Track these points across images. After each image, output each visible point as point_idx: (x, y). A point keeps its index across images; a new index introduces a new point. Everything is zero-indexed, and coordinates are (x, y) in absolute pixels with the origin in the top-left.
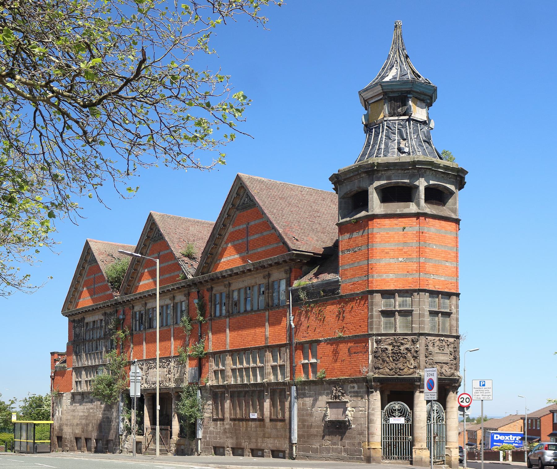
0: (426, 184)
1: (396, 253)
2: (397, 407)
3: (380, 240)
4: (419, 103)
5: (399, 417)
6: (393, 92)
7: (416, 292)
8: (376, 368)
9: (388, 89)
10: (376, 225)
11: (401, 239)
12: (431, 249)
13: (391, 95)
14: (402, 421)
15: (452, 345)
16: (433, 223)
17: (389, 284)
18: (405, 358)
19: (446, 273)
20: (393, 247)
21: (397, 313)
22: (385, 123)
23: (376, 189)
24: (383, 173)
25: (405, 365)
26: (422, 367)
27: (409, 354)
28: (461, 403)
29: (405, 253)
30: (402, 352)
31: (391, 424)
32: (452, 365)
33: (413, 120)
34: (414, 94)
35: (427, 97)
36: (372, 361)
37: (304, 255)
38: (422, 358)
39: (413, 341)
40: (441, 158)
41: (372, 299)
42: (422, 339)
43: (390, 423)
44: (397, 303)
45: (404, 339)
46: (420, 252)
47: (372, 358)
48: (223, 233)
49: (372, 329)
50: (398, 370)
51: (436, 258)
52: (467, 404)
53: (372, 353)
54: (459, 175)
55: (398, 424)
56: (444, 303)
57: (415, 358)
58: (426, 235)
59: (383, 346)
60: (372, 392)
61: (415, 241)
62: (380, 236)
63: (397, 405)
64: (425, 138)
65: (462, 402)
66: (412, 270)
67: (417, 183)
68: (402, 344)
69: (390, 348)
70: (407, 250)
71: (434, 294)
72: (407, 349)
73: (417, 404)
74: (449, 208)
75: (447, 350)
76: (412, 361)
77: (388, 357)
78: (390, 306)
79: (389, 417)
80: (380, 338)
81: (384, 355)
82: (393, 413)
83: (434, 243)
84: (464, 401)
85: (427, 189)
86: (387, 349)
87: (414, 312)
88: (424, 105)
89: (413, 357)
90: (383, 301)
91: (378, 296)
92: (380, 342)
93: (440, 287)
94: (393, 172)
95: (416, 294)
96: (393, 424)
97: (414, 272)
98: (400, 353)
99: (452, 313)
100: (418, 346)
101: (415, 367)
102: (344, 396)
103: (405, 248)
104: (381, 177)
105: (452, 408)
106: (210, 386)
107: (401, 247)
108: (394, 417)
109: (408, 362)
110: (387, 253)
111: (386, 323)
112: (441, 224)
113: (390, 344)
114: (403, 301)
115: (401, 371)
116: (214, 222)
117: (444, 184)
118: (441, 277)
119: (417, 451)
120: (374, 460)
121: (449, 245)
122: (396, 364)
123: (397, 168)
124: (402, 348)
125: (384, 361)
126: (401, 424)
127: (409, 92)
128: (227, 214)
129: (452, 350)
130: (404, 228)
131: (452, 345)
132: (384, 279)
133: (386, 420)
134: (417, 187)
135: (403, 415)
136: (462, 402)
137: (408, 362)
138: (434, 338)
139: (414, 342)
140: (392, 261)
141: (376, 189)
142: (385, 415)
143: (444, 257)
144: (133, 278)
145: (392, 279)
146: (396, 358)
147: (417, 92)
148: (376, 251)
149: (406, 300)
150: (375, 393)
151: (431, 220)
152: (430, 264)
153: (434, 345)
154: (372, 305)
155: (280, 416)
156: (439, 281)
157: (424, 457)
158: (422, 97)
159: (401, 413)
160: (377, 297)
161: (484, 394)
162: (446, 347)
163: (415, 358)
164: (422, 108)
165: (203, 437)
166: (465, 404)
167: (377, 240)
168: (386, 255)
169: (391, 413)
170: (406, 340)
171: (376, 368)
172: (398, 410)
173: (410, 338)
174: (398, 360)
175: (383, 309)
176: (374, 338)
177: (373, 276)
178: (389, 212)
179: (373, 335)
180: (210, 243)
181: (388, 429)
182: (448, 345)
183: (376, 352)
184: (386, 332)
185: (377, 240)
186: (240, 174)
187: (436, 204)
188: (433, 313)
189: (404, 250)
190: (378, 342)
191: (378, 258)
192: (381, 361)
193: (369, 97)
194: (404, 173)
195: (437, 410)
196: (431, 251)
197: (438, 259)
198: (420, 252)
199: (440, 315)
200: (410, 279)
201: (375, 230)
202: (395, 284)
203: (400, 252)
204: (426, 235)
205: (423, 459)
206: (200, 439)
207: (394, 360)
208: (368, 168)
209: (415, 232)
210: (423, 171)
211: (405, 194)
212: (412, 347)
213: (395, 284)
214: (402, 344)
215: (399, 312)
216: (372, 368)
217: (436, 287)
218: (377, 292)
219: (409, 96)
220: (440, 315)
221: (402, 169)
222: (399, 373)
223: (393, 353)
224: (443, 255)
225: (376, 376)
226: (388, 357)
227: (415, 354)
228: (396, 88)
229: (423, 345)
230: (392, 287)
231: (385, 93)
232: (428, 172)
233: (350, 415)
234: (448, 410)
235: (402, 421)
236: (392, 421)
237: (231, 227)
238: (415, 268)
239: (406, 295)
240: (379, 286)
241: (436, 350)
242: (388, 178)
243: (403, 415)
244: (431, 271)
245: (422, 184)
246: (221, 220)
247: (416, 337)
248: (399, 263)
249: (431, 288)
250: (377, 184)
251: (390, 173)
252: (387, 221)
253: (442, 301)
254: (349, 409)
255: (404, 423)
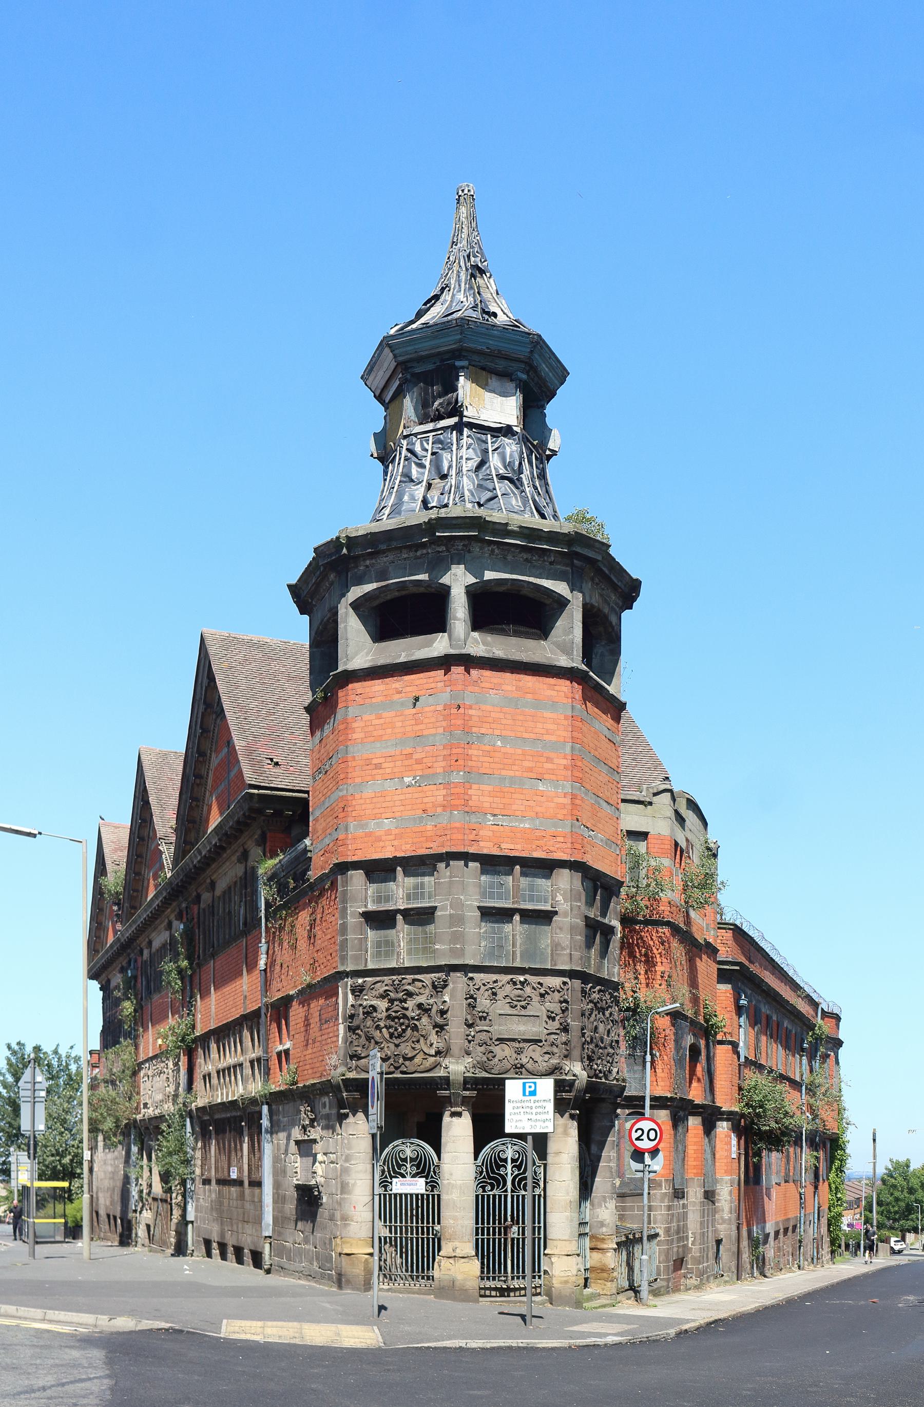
0: (472, 580)
1: (399, 763)
2: (409, 1152)
3: (362, 735)
4: (494, 382)
5: (414, 1176)
6: (421, 359)
7: (441, 861)
8: (352, 1057)
9: (407, 353)
10: (353, 697)
11: (408, 729)
12: (487, 748)
13: (418, 370)
14: (419, 1186)
15: (557, 996)
16: (495, 681)
17: (382, 844)
18: (415, 1028)
19: (538, 809)
20: (391, 751)
21: (399, 917)
22: (404, 442)
23: (356, 606)
24: (368, 562)
25: (417, 1046)
26: (455, 1050)
27: (425, 1020)
28: (638, 1143)
29: (419, 762)
30: (410, 1014)
31: (395, 1195)
32: (552, 1044)
33: (471, 426)
34: (475, 357)
35: (515, 365)
36: (345, 1040)
37: (276, 796)
38: (456, 1029)
39: (434, 987)
40: (543, 516)
41: (346, 883)
42: (458, 981)
43: (394, 1191)
44: (401, 892)
45: (414, 980)
46: (456, 758)
47: (345, 1033)
48: (203, 772)
49: (343, 959)
50: (401, 1061)
51: (504, 773)
52: (651, 1145)
53: (345, 1020)
54: (577, 554)
55: (411, 1195)
56: (531, 888)
57: (440, 1028)
58: (471, 712)
59: (368, 1000)
60: (346, 1116)
61: (441, 730)
62: (362, 724)
63: (408, 1148)
64: (502, 471)
65: (638, 1139)
66: (435, 806)
67: (445, 580)
68: (410, 994)
69: (382, 1005)
70: (423, 755)
71: (494, 864)
72: (420, 1006)
73: (446, 1144)
74: (558, 645)
75: (537, 1008)
76: (433, 1038)
77: (378, 1028)
78: (387, 899)
79: (391, 1177)
80: (360, 981)
81: (369, 1023)
82: (399, 1167)
83: (497, 732)
84: (645, 1137)
85: (476, 595)
86: (374, 1009)
87: (438, 913)
88: (511, 386)
89: (434, 1027)
90: (372, 888)
91: (357, 876)
92: (361, 991)
93: (519, 847)
94: (391, 557)
95: (443, 865)
96: (401, 1195)
97: (439, 810)
98: (405, 1016)
99: (556, 913)
100: (446, 998)
101: (438, 1053)
102: (313, 1127)
103: (419, 749)
104: (365, 573)
105: (558, 1153)
106: (198, 1109)
107: (409, 750)
108: (403, 1176)
109: (422, 1040)
110: (378, 766)
111: (378, 944)
112: (521, 684)
113: (382, 997)
114: (416, 887)
115: (407, 1063)
116: (183, 750)
117: (531, 579)
118: (521, 822)
119: (445, 1263)
120: (348, 1281)
121: (546, 737)
122: (397, 1046)
123: (394, 544)
124: (410, 1004)
125: (369, 1038)
126: (417, 1195)
127: (458, 353)
128: (201, 728)
129: (556, 1008)
130: (417, 699)
131: (557, 996)
132: (370, 834)
133: (385, 1184)
134: (446, 590)
135: (423, 1171)
136: (638, 1139)
137: (422, 1040)
138: (495, 977)
139: (438, 988)
140: (389, 785)
141: (356, 606)
142: (383, 1171)
143: (530, 770)
144: (137, 891)
145: (388, 832)
146: (396, 1029)
147: (480, 353)
148: (354, 764)
149: (422, 884)
150: (351, 1119)
151: (487, 673)
152: (483, 787)
153: (494, 994)
154: (344, 901)
155: (234, 1176)
156: (513, 830)
157: (459, 1277)
158: (501, 365)
159: (418, 1167)
160: (355, 880)
161: (534, 1117)
162: (536, 999)
163: (440, 1028)
164: (504, 394)
165: (196, 1217)
166: (645, 1144)
167: (355, 736)
168: (375, 772)
169: (394, 1169)
170: (420, 984)
171: (352, 1057)
172: (412, 1160)
173: (427, 978)
174: (400, 1036)
175: (371, 907)
176: (350, 981)
177: (346, 829)
178: (381, 662)
179: (347, 974)
180: (184, 797)
181: (388, 1206)
182: (542, 995)
183: (352, 1017)
184: (377, 967)
185: (355, 736)
186: (205, 630)
187: (517, 634)
188: (489, 914)
189: (416, 756)
190: (358, 991)
191: (358, 780)
192: (363, 1039)
193: (381, 386)
194: (417, 558)
195: (513, 1161)
196: (488, 754)
197: (511, 773)
198: (456, 758)
199: (517, 918)
200: (429, 827)
201: (352, 711)
202: (396, 843)
203: (406, 763)
204: (471, 712)
205: (457, 1284)
206: (192, 1222)
207: (391, 1035)
208: (331, 555)
209: (440, 708)
210: (460, 545)
211: (428, 613)
212: (431, 1001)
213: (396, 843)
214: (410, 994)
215: (406, 913)
216: (345, 1056)
217: (503, 846)
218: (356, 865)
219: (458, 363)
220: (517, 918)
221: (409, 548)
222: (403, 1069)
223: (389, 1017)
224: (527, 764)
225: (352, 1075)
226: (378, 1028)
227: (439, 1020)
228: (425, 348)
229: (461, 995)
230: (388, 853)
231: (403, 366)
232: (476, 548)
233: (320, 1172)
234: (550, 1159)
235: (419, 1186)
236: (399, 1186)
237: (213, 755)
238: (440, 799)
239: (422, 869)
240: (359, 853)
241: (502, 1006)
242: (382, 575)
243: (423, 1171)
244: (486, 805)
245: (458, 580)
246: (194, 742)
247: (442, 975)
248: (406, 790)
249: (487, 848)
250: (356, 592)
251: (383, 560)
252: (377, 687)
253: (524, 882)
254: (320, 1157)
255: (423, 1191)
